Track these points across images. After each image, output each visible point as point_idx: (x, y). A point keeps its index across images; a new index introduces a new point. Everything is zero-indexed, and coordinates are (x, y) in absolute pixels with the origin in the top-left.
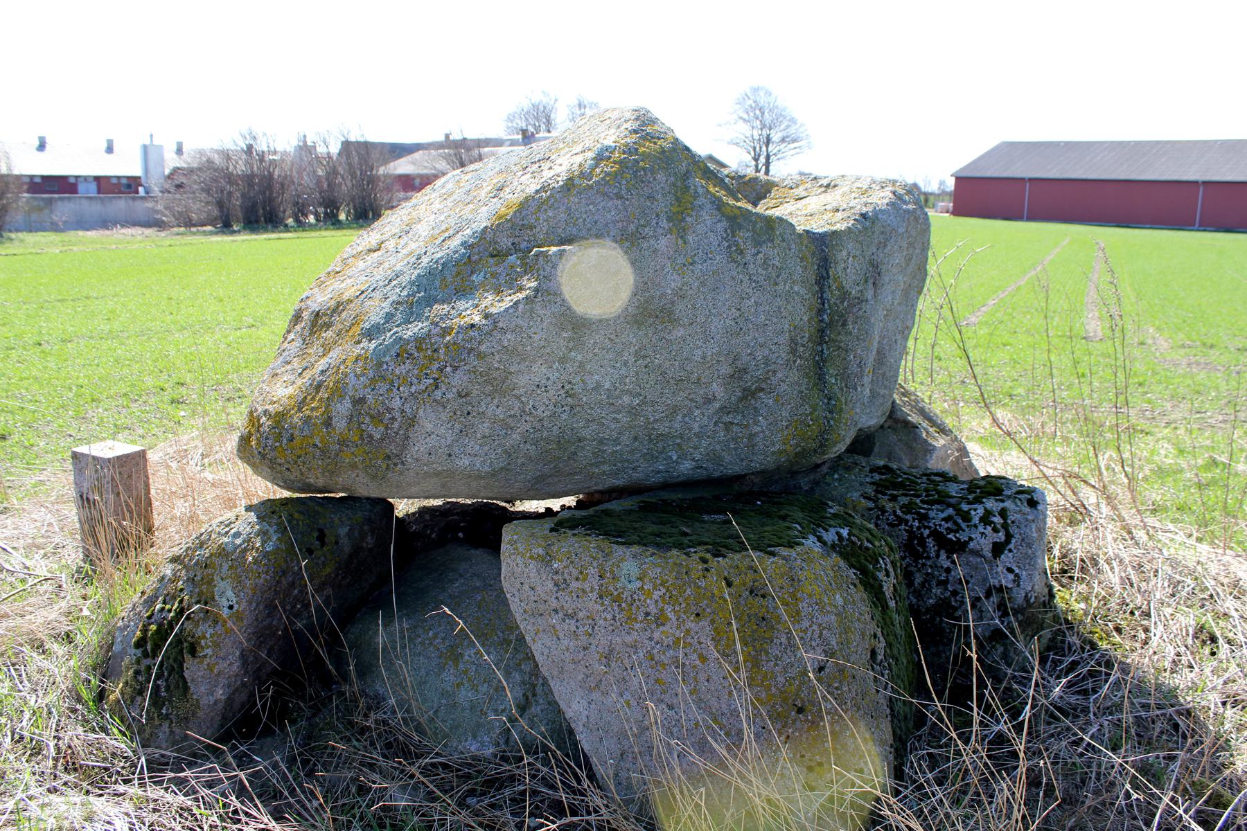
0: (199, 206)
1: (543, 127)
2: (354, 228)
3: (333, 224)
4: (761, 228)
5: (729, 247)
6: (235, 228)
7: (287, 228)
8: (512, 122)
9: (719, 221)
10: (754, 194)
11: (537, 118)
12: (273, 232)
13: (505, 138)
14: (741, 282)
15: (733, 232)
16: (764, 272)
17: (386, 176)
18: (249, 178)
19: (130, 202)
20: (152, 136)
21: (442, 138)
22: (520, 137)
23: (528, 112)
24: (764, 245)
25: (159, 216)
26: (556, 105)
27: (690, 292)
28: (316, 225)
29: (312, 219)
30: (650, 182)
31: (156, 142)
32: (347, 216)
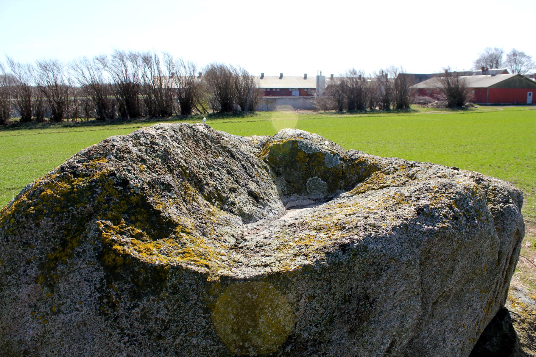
0: (330, 103)
1: (494, 65)
2: (396, 113)
3: (387, 111)
4: (146, 279)
5: (101, 298)
6: (344, 111)
7: (366, 112)
8: (479, 64)
9: (97, 270)
10: (357, 176)
11: (491, 61)
12: (359, 113)
13: (474, 71)
14: (110, 335)
15: (110, 283)
16: (142, 326)
17: (413, 89)
18: (352, 91)
19: (305, 100)
20: (321, 72)
21: (443, 72)
22: (481, 71)
23: (487, 59)
24: (145, 299)
25: (314, 106)
26: (502, 55)
27: (53, 340)
28: (379, 111)
29: (377, 108)
30: (31, 229)
31: (322, 75)
32: (393, 107)
